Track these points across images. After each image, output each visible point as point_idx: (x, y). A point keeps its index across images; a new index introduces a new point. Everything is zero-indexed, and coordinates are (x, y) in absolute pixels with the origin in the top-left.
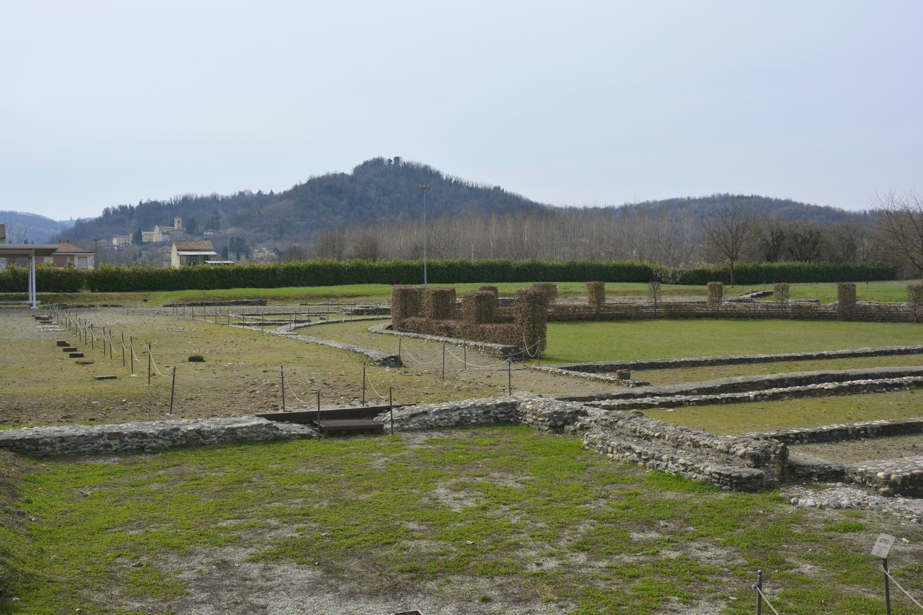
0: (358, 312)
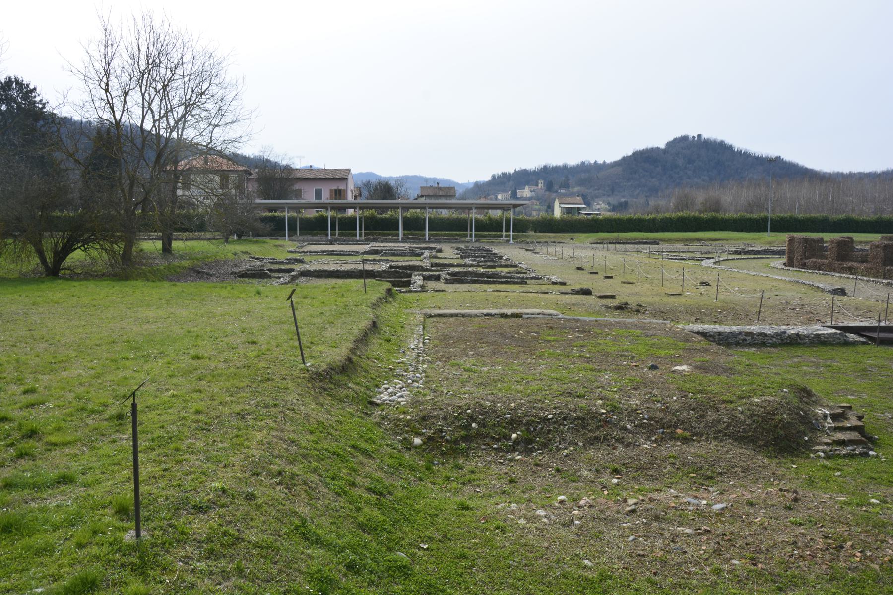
0: (736, 253)
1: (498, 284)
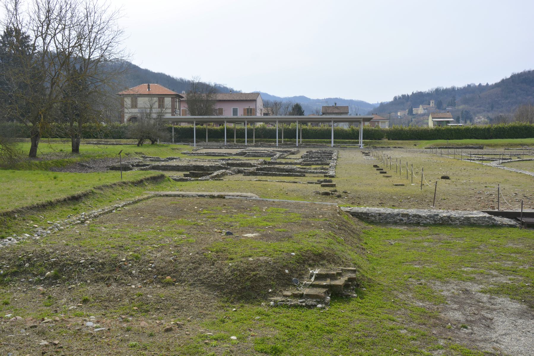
1: (283, 176)
